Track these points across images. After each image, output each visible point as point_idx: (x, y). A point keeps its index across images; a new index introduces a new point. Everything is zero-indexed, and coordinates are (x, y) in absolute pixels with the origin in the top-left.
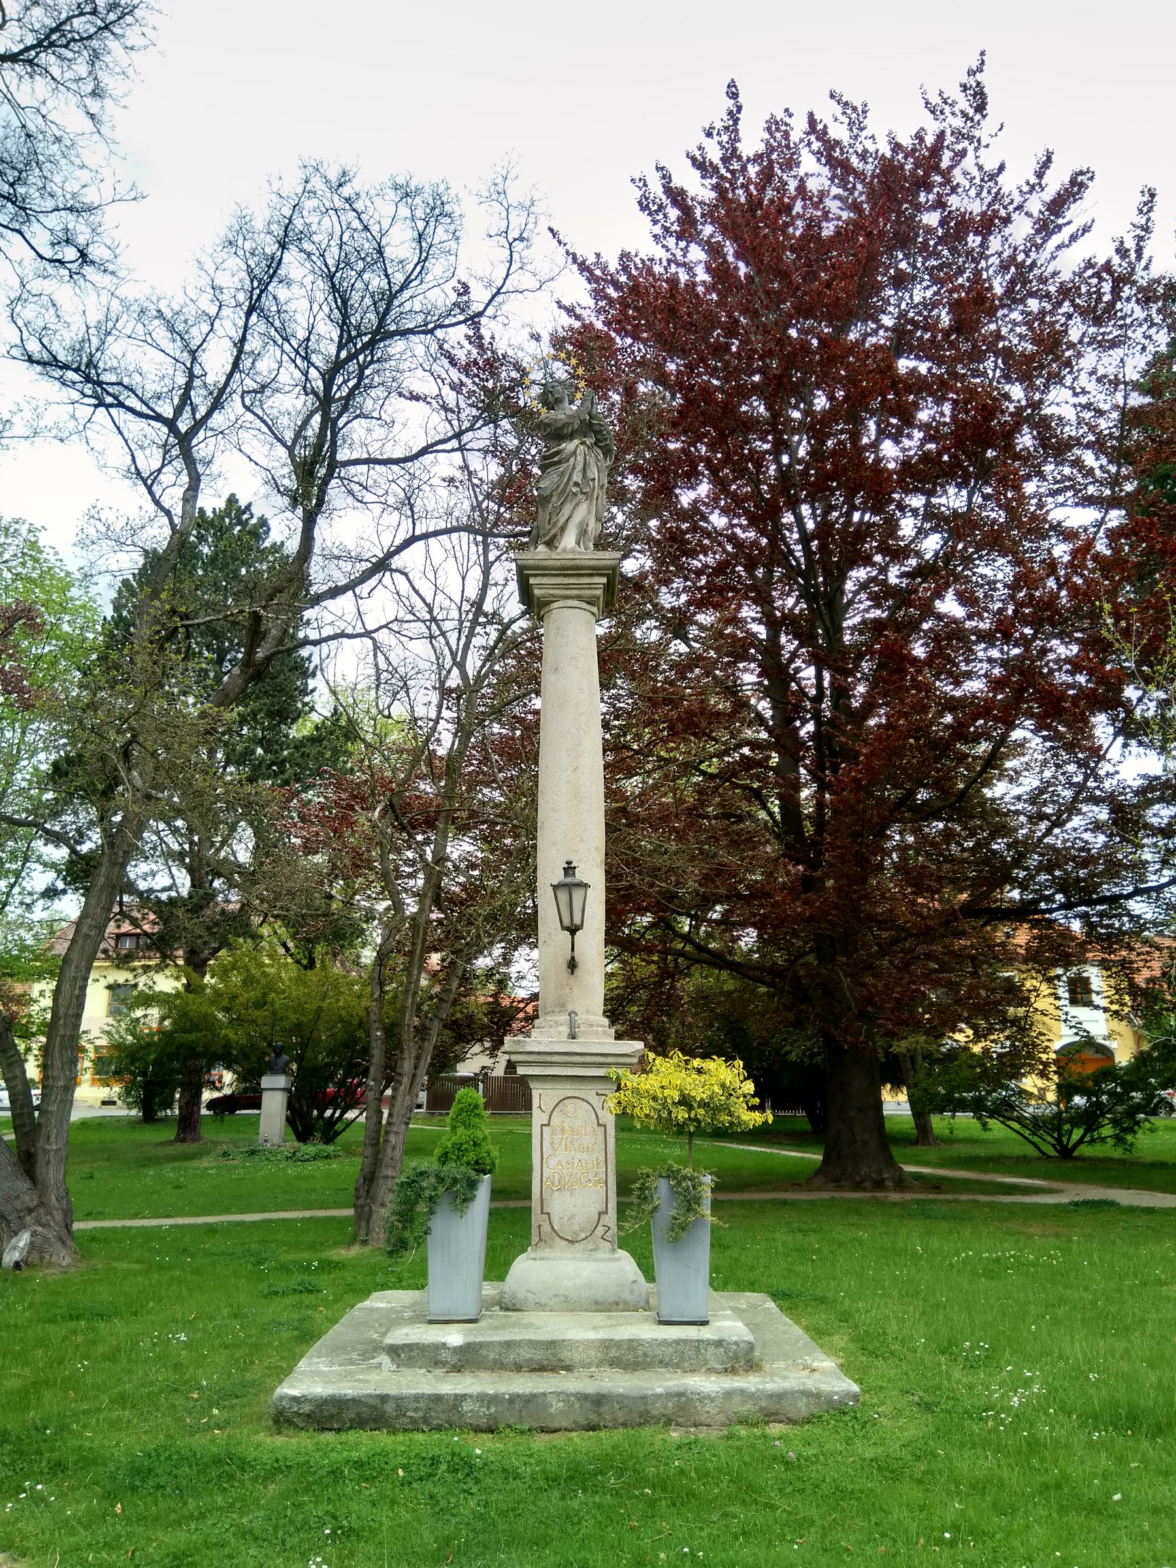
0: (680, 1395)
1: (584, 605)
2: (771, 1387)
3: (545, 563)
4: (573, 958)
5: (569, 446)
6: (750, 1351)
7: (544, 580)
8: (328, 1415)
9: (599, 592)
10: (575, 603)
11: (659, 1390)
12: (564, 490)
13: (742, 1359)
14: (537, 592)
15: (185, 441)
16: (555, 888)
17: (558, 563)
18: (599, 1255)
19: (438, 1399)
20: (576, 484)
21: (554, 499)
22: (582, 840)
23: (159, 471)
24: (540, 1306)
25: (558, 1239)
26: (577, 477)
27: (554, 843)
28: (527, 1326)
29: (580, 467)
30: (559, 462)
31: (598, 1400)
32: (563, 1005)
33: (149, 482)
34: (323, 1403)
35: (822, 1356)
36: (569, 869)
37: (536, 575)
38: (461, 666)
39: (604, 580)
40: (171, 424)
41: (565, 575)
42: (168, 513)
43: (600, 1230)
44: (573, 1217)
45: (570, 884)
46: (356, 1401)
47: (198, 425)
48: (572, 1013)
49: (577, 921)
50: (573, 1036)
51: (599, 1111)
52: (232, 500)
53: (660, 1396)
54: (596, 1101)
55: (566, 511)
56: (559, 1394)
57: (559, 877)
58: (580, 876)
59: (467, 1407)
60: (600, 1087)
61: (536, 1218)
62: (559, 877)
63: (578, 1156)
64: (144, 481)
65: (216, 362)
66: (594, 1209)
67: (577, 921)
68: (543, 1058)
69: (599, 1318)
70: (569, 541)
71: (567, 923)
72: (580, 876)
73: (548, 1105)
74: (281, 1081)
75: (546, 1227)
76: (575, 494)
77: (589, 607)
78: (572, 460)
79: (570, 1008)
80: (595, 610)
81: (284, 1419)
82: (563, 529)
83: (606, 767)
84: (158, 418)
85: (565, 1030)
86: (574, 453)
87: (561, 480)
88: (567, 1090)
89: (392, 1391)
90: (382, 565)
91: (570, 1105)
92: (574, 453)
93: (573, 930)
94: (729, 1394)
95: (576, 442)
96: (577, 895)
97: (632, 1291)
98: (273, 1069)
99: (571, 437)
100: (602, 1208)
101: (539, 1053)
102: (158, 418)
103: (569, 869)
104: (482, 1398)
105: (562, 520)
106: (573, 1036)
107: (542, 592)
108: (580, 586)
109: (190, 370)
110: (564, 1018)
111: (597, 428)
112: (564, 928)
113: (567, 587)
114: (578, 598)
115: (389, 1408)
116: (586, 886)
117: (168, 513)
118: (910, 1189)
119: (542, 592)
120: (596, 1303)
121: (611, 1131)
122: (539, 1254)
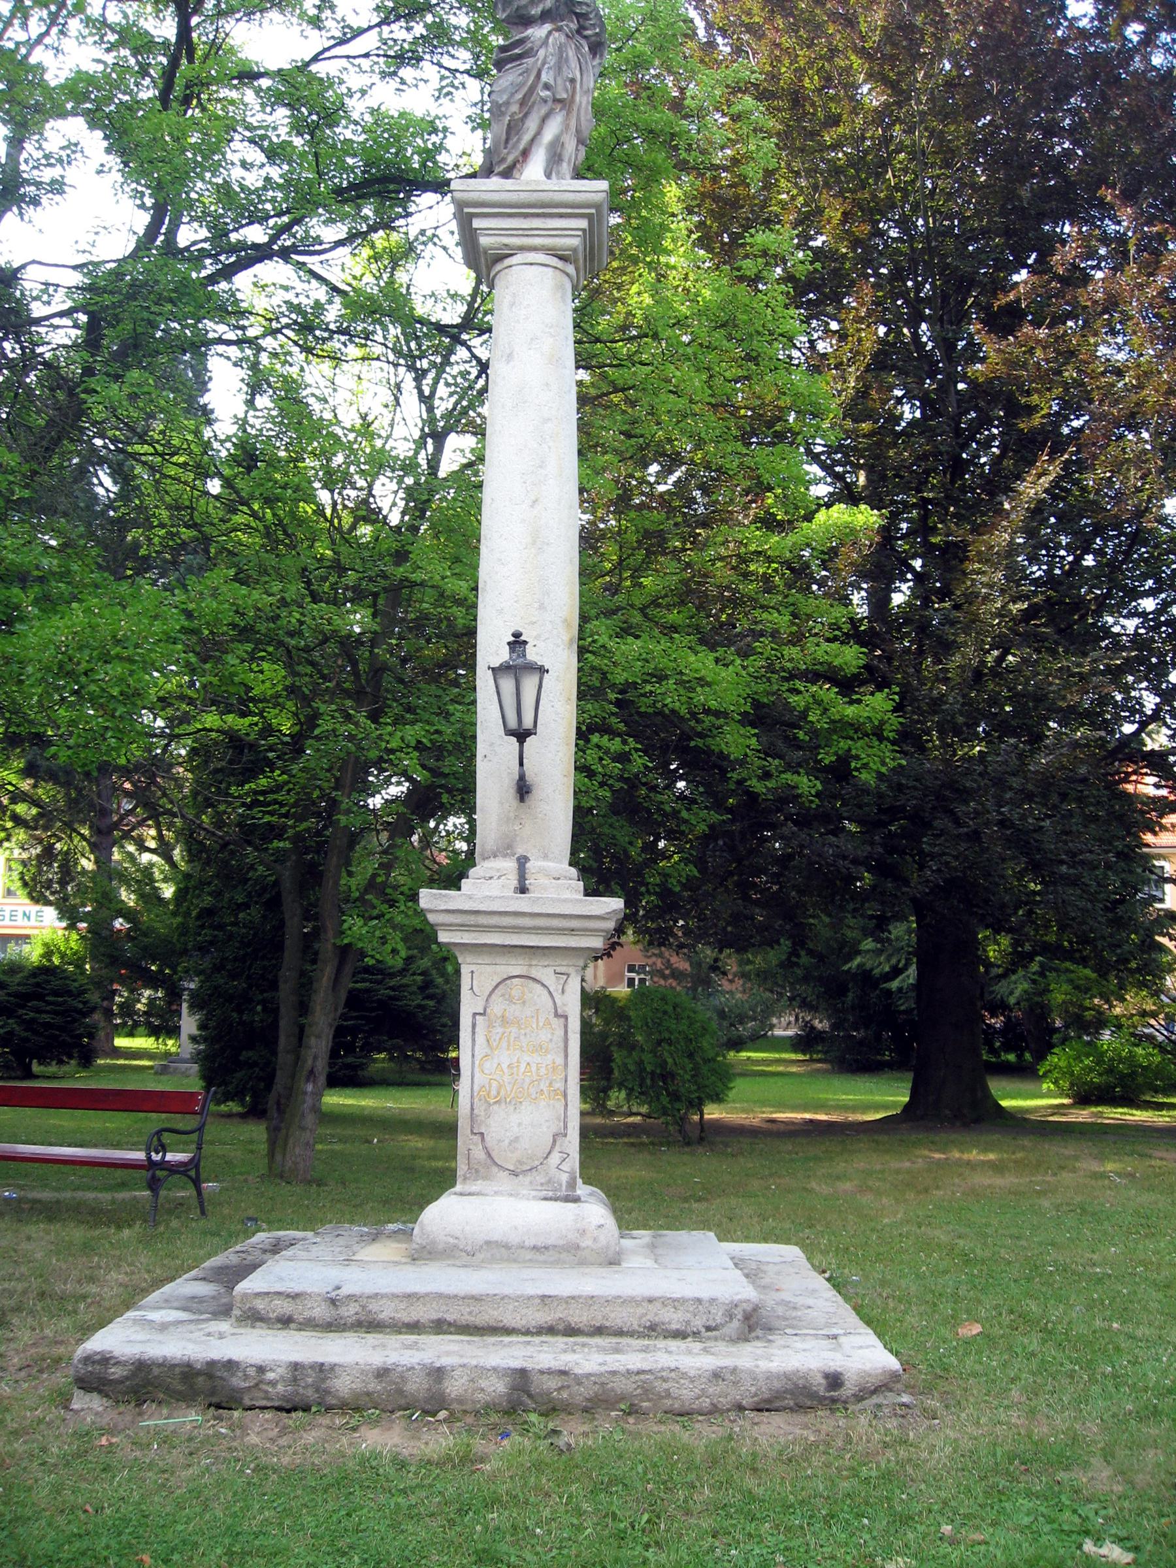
1: (555, 262)
4: (522, 777)
5: (538, 32)
6: (748, 1308)
8: (144, 1384)
10: (540, 257)
20: (547, 87)
27: (500, 611)
30: (520, 57)
32: (509, 846)
34: (142, 1367)
36: (517, 643)
41: (526, 216)
44: (517, 1139)
45: (519, 665)
48: (522, 862)
49: (528, 722)
55: (532, 124)
58: (532, 654)
62: (503, 655)
63: (527, 1058)
67: (528, 722)
68: (473, 918)
71: (513, 723)
72: (532, 654)
75: (479, 1154)
79: (520, 851)
80: (571, 269)
81: (95, 1377)
82: (525, 153)
83: (575, 310)
85: (514, 882)
88: (516, 967)
92: (545, 42)
93: (522, 735)
96: (529, 685)
100: (556, 1127)
101: (549, 915)
103: (517, 643)
105: (527, 138)
106: (523, 890)
110: (510, 865)
112: (510, 732)
116: (542, 670)
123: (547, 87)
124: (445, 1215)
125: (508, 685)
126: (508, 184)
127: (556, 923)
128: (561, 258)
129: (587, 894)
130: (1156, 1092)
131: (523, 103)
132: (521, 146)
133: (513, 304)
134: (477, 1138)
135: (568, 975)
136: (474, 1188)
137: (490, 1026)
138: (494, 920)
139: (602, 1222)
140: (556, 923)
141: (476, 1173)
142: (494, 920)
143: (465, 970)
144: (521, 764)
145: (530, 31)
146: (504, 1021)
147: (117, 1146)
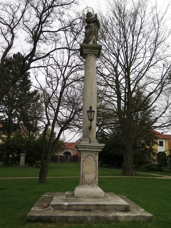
0: (116, 217)
1: (94, 56)
2: (134, 215)
3: (87, 46)
7: (86, 50)
9: (97, 53)
10: (92, 55)
11: (111, 216)
12: (90, 33)
13: (126, 209)
14: (84, 52)
15: (12, 29)
16: (88, 111)
17: (89, 46)
18: (94, 187)
19: (63, 217)
20: (93, 32)
21: (88, 35)
22: (93, 103)
23: (6, 33)
24: (83, 197)
25: (86, 184)
26: (93, 30)
27: (87, 103)
28: (81, 201)
29: (94, 28)
30: (89, 27)
31: (98, 218)
33: (4, 35)
35: (140, 208)
37: (84, 49)
38: (63, 75)
39: (98, 51)
40: (9, 26)
42: (8, 41)
43: (95, 182)
46: (45, 217)
47: (15, 27)
48: (90, 138)
49: (92, 118)
50: (90, 142)
51: (95, 158)
52: (18, 52)
53: (111, 217)
54: (94, 156)
55: (91, 37)
56: (90, 216)
57: (88, 109)
59: (70, 219)
60: (95, 153)
61: (81, 179)
62: (88, 109)
64: (4, 35)
65: (19, 14)
66: (93, 178)
69: (95, 200)
70: (91, 43)
71: (90, 118)
73: (84, 156)
74: (24, 154)
75: (83, 181)
76: (93, 34)
77: (95, 56)
78: (92, 27)
79: (89, 137)
82: (90, 41)
84: (7, 25)
85: (88, 141)
86: (92, 26)
87: (90, 31)
89: (53, 215)
90: (48, 54)
91: (89, 157)
94: (126, 217)
95: (93, 24)
96: (92, 113)
97: (101, 194)
98: (22, 152)
99: (92, 23)
100: (95, 177)
102: (7, 25)
103: (91, 108)
104: (73, 217)
105: (90, 39)
107: (86, 52)
108: (93, 52)
109: (14, 16)
110: (88, 139)
111: (97, 21)
112: (89, 120)
113: (91, 51)
114: (93, 54)
115: (53, 219)
117: (8, 41)
118: (138, 176)
119: (86, 52)
120: (94, 197)
121: (97, 162)
122: (82, 187)
123: (93, 32)
124: (79, 190)
125: (89, 114)
126: (86, 44)
127: (96, 147)
128: (95, 55)
129: (99, 143)
130: (117, 211)
131: (90, 34)
132: (89, 40)
133: (88, 61)
134: (83, 179)
135: (96, 155)
136: (83, 187)
137: (85, 162)
138: (86, 147)
139: (102, 192)
140: (98, 147)
141: (83, 184)
142: (86, 147)
143: (82, 154)
144: (91, 124)
145: (90, 24)
146: (87, 161)
147: (115, 177)
